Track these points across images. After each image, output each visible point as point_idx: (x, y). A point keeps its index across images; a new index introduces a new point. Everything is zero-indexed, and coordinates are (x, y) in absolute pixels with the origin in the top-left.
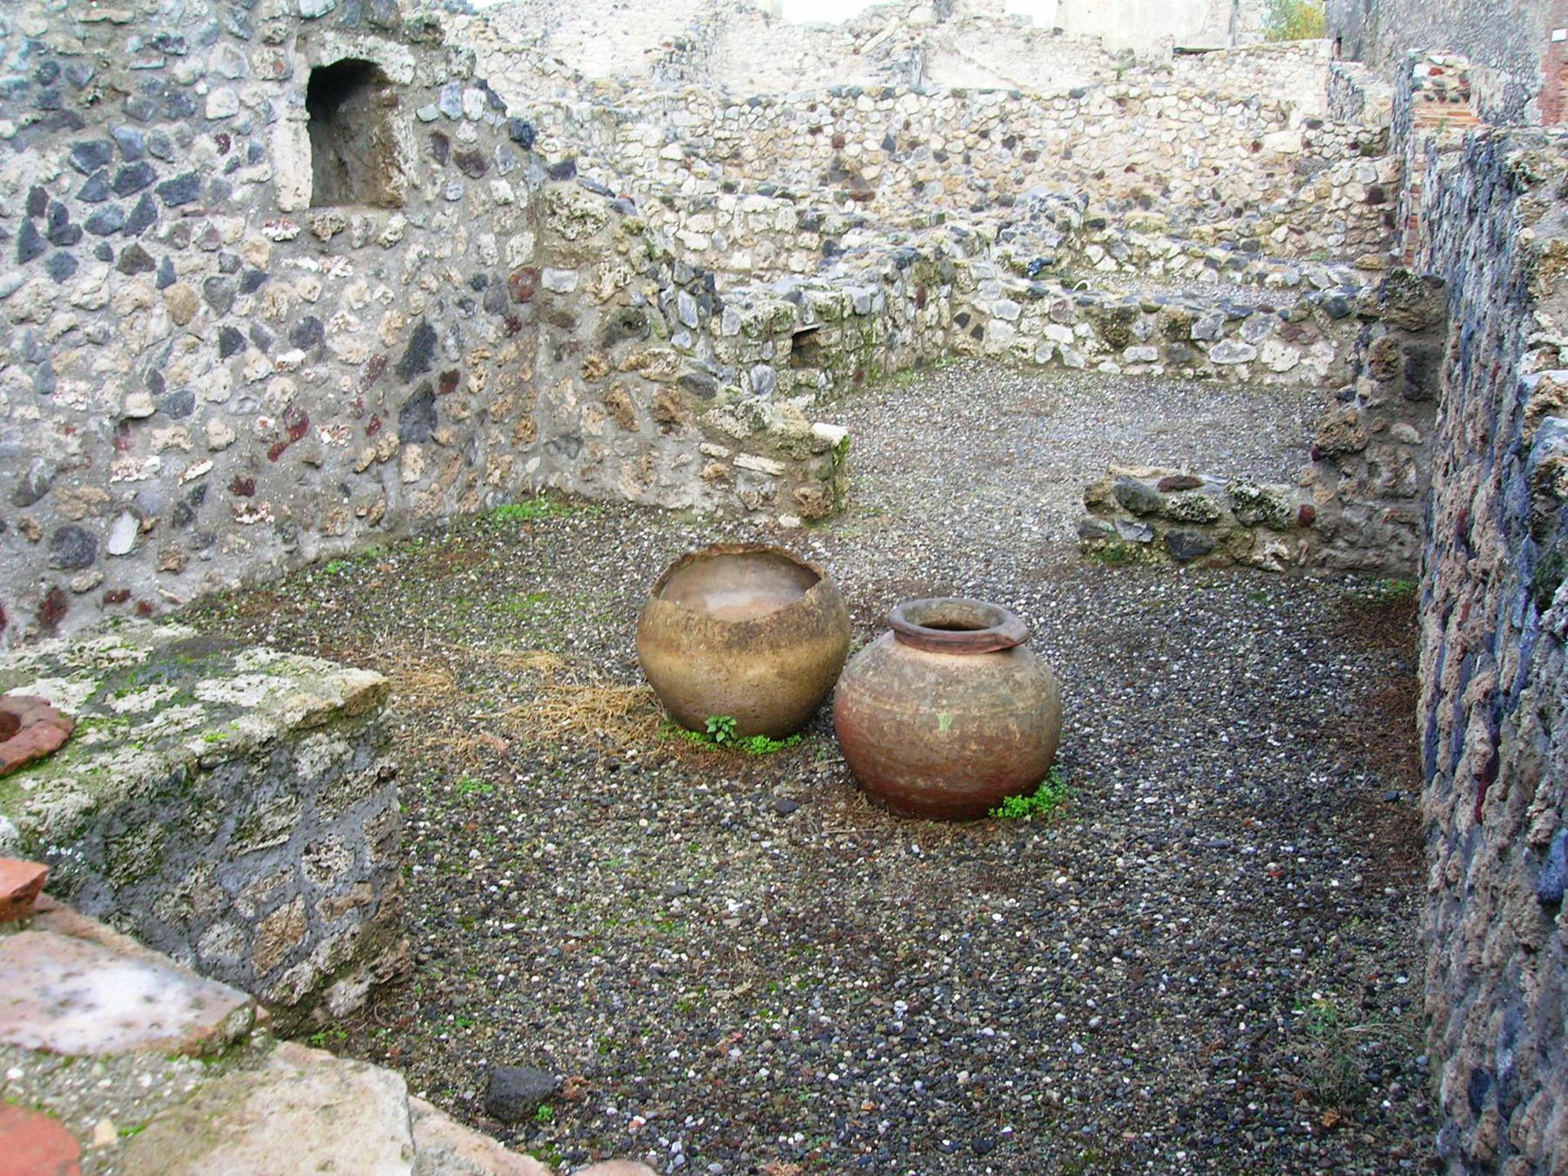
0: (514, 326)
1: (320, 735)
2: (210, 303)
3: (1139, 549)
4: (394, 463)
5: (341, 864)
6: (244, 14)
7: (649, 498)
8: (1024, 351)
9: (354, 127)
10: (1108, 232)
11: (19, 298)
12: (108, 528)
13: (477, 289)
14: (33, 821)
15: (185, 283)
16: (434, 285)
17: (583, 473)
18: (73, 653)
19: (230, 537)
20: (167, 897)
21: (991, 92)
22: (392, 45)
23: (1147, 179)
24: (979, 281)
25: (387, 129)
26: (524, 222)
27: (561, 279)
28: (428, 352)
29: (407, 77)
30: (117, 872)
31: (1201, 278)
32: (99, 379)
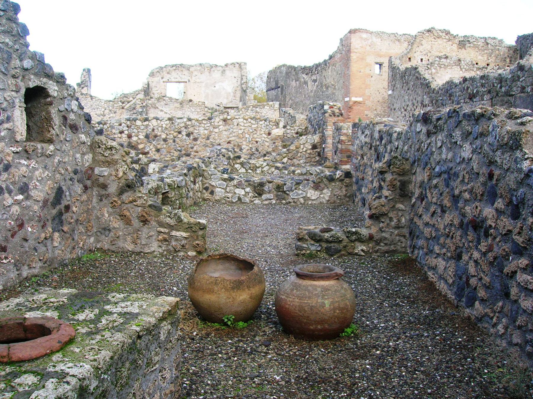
0: (86, 188)
3: (317, 253)
4: (50, 239)
6: (6, 65)
7: (138, 250)
8: (228, 198)
9: (34, 112)
10: (242, 159)
14: (95, 363)
17: (111, 242)
21: (181, 118)
22: (51, 82)
23: (235, 146)
24: (212, 175)
25: (49, 113)
26: (89, 150)
27: (102, 171)
29: (56, 94)
31: (274, 173)
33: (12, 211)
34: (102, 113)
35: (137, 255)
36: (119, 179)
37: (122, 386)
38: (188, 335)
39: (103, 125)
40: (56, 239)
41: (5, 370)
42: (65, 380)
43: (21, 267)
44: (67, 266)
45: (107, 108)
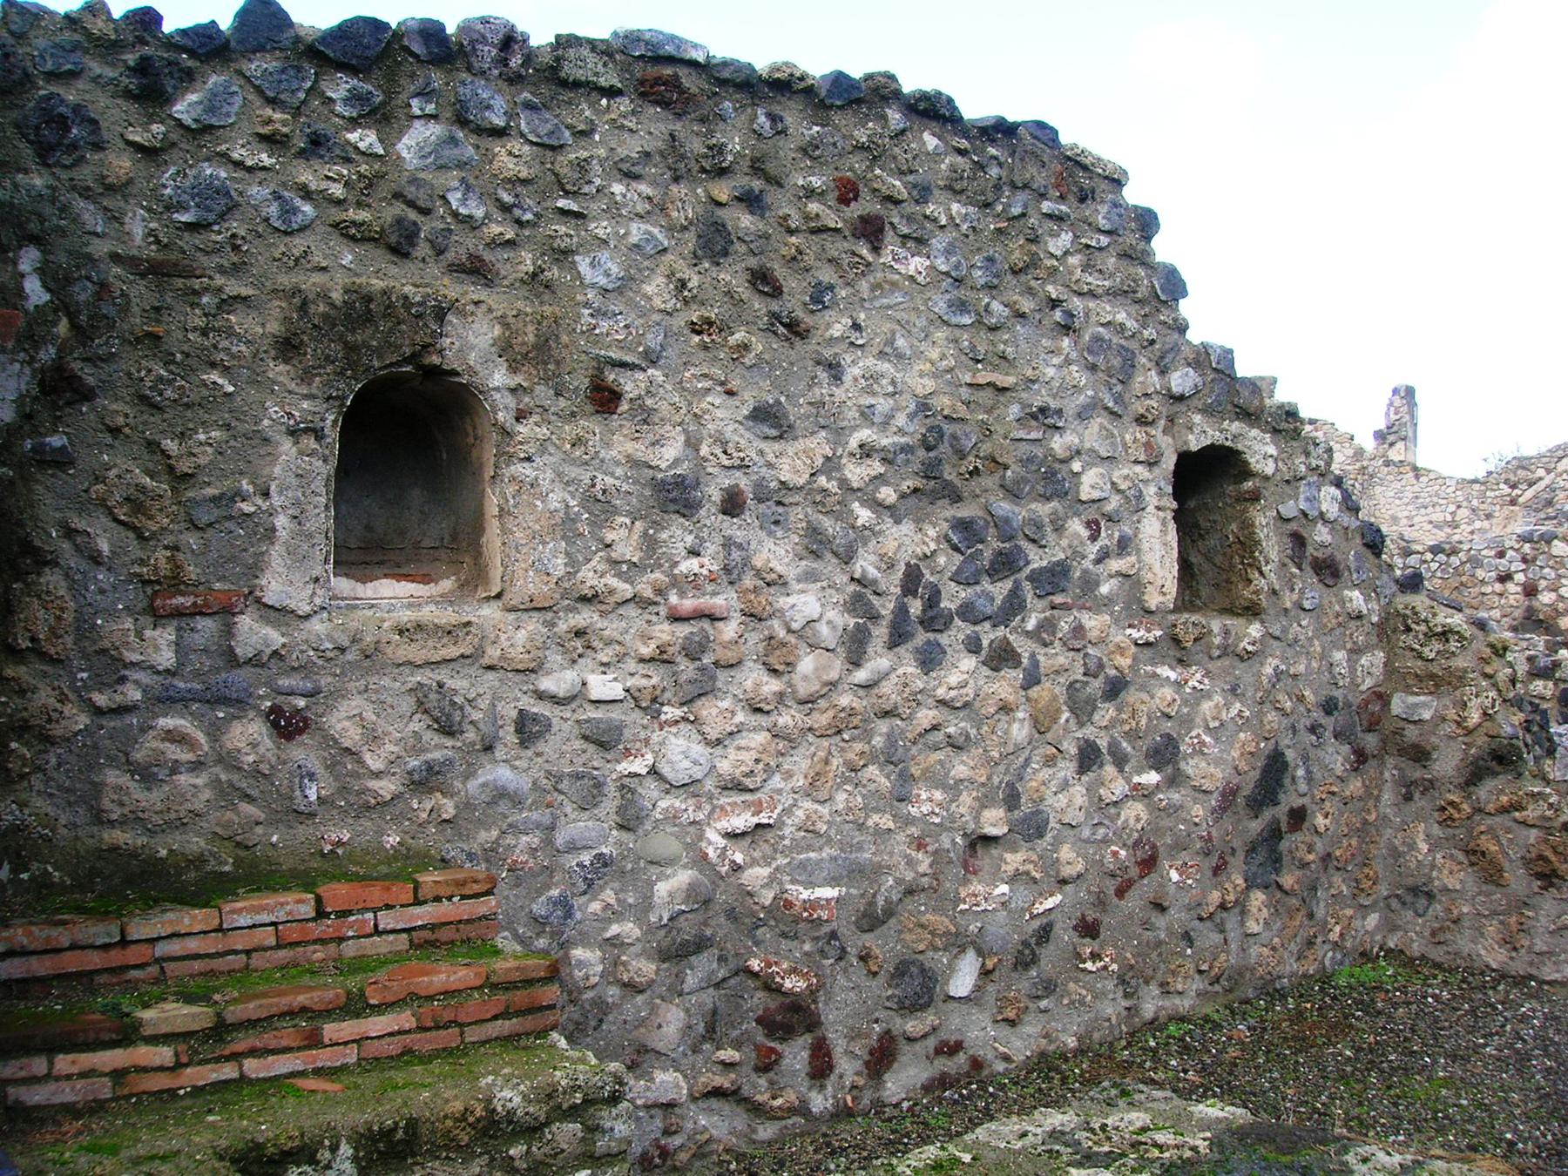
0: (1361, 757)
2: (1072, 711)
4: (1237, 910)
6: (1119, 388)
7: (1519, 967)
9: (1204, 524)
11: (886, 688)
15: (1048, 685)
17: (1433, 934)
19: (1071, 985)
22: (1255, 432)
25: (1247, 525)
26: (1375, 640)
27: (1416, 705)
29: (1269, 469)
34: (1449, 518)
35: (1516, 984)
36: (1469, 732)
39: (1448, 556)
40: (1254, 910)
43: (1138, 985)
44: (1284, 997)
45: (1465, 504)
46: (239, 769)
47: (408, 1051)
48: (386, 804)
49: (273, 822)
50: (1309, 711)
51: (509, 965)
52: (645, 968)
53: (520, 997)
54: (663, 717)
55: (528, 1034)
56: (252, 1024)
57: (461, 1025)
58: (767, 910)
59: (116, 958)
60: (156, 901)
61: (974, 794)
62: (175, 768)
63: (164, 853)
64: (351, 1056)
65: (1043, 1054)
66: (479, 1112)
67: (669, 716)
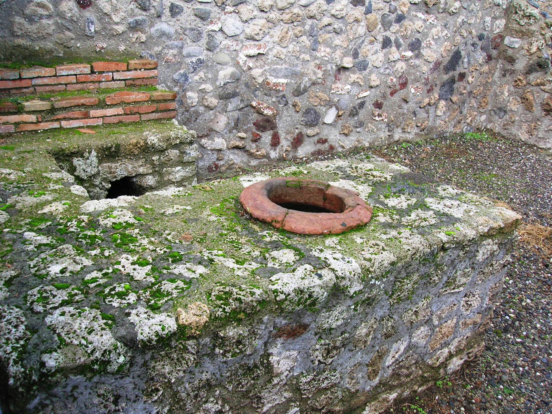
0: (490, 58)
1: (490, 240)
2: (382, 25)
4: (434, 106)
5: (476, 304)
7: (532, 142)
11: (312, 8)
12: (326, 112)
13: (480, 40)
14: (368, 264)
15: (375, 14)
16: (465, 35)
17: (504, 126)
18: (352, 168)
19: (369, 124)
20: (410, 311)
26: (503, 15)
27: (513, 42)
28: (457, 63)
30: (394, 296)
32: (335, 48)
33: (396, 67)
35: (529, 147)
36: (531, 55)
37: (400, 299)
38: (543, 259)
41: (271, 237)
42: (319, 272)
46: (65, 18)
47: (120, 122)
48: (120, 34)
49: (78, 39)
50: (473, 38)
51: (158, 94)
52: (213, 101)
53: (162, 106)
54: (226, 10)
55: (164, 119)
56: (64, 109)
57: (140, 114)
58: (261, 85)
59: (18, 84)
60: (33, 65)
61: (342, 51)
62: (41, 17)
63: (37, 48)
64: (100, 122)
65: (356, 147)
66: (142, 143)
67: (228, 10)
